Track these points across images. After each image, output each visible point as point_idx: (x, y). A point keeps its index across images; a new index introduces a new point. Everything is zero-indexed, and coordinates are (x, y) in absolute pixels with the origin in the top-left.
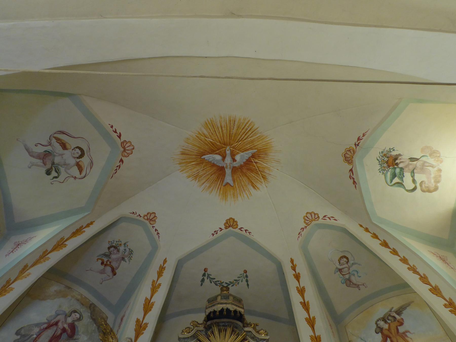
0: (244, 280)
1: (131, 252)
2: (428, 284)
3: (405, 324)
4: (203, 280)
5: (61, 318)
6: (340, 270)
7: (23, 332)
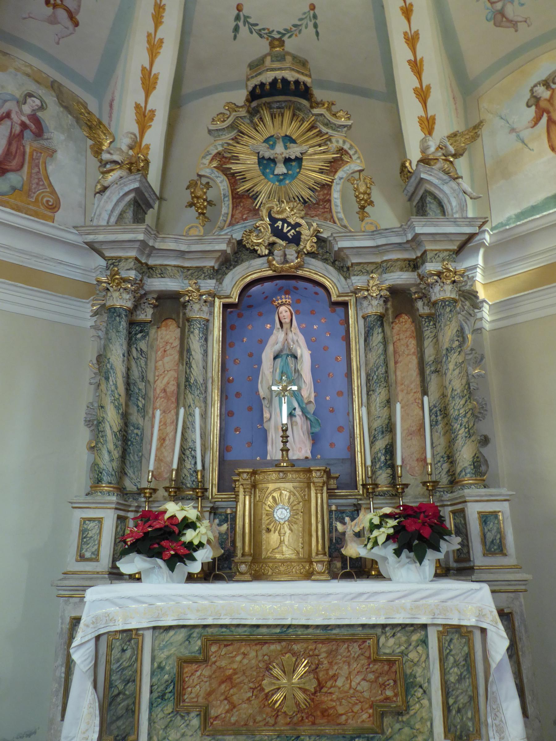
4: (236, 29)
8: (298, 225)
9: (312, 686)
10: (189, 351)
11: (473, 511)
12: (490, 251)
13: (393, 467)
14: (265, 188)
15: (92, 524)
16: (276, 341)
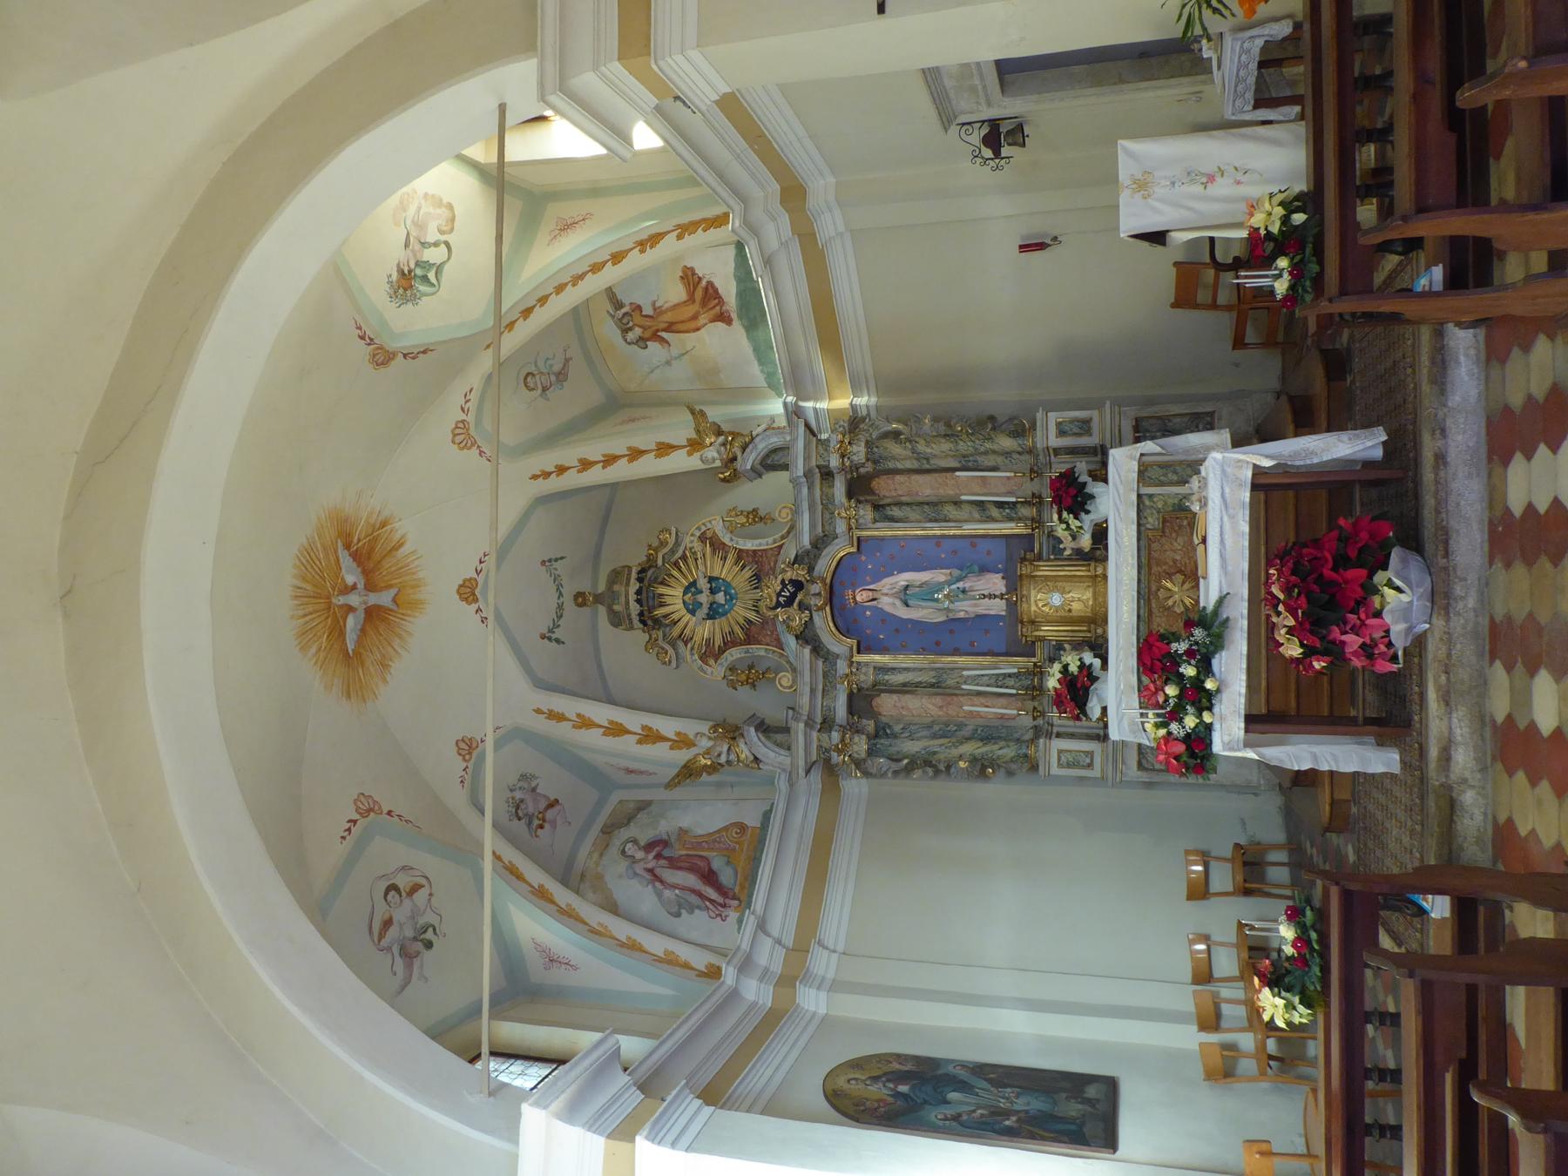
0: (555, 565)
1: (523, 777)
2: (605, 263)
4: (558, 641)
5: (639, 868)
6: (544, 389)
7: (675, 909)
8: (783, 581)
9: (1180, 577)
10: (904, 685)
14: (741, 612)
16: (889, 604)
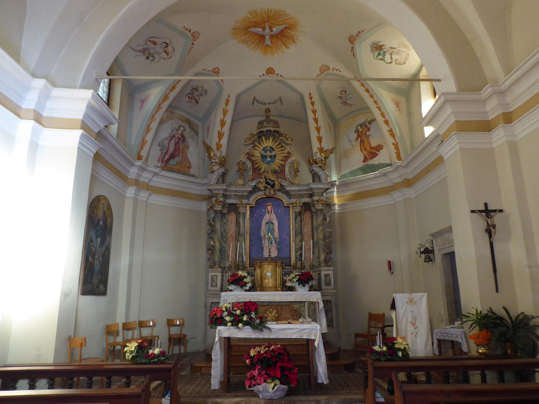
0: (280, 102)
2: (384, 117)
3: (371, 130)
4: (253, 103)
5: (175, 132)
6: (341, 97)
7: (161, 144)
8: (274, 181)
11: (323, 273)
12: (337, 186)
13: (302, 260)
14: (264, 166)
15: (214, 277)
16: (267, 217)
